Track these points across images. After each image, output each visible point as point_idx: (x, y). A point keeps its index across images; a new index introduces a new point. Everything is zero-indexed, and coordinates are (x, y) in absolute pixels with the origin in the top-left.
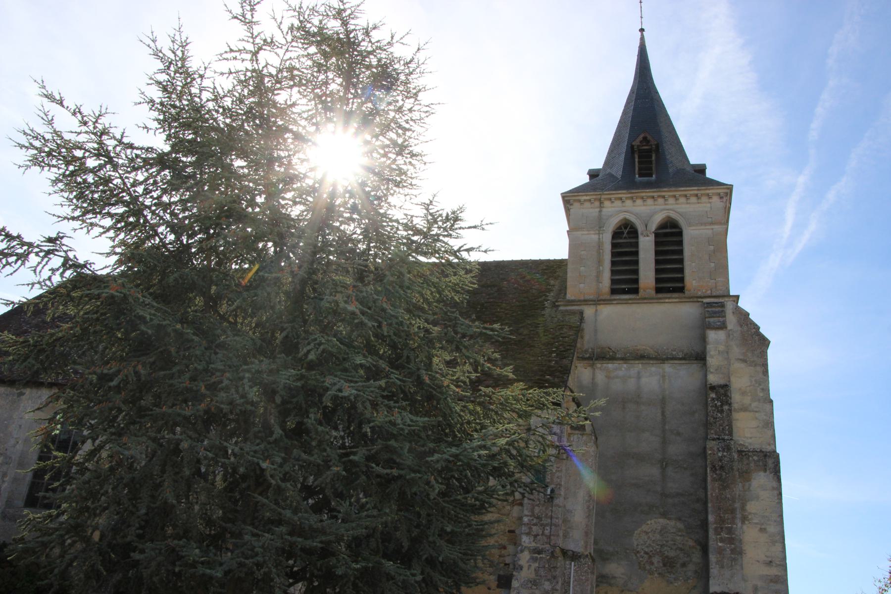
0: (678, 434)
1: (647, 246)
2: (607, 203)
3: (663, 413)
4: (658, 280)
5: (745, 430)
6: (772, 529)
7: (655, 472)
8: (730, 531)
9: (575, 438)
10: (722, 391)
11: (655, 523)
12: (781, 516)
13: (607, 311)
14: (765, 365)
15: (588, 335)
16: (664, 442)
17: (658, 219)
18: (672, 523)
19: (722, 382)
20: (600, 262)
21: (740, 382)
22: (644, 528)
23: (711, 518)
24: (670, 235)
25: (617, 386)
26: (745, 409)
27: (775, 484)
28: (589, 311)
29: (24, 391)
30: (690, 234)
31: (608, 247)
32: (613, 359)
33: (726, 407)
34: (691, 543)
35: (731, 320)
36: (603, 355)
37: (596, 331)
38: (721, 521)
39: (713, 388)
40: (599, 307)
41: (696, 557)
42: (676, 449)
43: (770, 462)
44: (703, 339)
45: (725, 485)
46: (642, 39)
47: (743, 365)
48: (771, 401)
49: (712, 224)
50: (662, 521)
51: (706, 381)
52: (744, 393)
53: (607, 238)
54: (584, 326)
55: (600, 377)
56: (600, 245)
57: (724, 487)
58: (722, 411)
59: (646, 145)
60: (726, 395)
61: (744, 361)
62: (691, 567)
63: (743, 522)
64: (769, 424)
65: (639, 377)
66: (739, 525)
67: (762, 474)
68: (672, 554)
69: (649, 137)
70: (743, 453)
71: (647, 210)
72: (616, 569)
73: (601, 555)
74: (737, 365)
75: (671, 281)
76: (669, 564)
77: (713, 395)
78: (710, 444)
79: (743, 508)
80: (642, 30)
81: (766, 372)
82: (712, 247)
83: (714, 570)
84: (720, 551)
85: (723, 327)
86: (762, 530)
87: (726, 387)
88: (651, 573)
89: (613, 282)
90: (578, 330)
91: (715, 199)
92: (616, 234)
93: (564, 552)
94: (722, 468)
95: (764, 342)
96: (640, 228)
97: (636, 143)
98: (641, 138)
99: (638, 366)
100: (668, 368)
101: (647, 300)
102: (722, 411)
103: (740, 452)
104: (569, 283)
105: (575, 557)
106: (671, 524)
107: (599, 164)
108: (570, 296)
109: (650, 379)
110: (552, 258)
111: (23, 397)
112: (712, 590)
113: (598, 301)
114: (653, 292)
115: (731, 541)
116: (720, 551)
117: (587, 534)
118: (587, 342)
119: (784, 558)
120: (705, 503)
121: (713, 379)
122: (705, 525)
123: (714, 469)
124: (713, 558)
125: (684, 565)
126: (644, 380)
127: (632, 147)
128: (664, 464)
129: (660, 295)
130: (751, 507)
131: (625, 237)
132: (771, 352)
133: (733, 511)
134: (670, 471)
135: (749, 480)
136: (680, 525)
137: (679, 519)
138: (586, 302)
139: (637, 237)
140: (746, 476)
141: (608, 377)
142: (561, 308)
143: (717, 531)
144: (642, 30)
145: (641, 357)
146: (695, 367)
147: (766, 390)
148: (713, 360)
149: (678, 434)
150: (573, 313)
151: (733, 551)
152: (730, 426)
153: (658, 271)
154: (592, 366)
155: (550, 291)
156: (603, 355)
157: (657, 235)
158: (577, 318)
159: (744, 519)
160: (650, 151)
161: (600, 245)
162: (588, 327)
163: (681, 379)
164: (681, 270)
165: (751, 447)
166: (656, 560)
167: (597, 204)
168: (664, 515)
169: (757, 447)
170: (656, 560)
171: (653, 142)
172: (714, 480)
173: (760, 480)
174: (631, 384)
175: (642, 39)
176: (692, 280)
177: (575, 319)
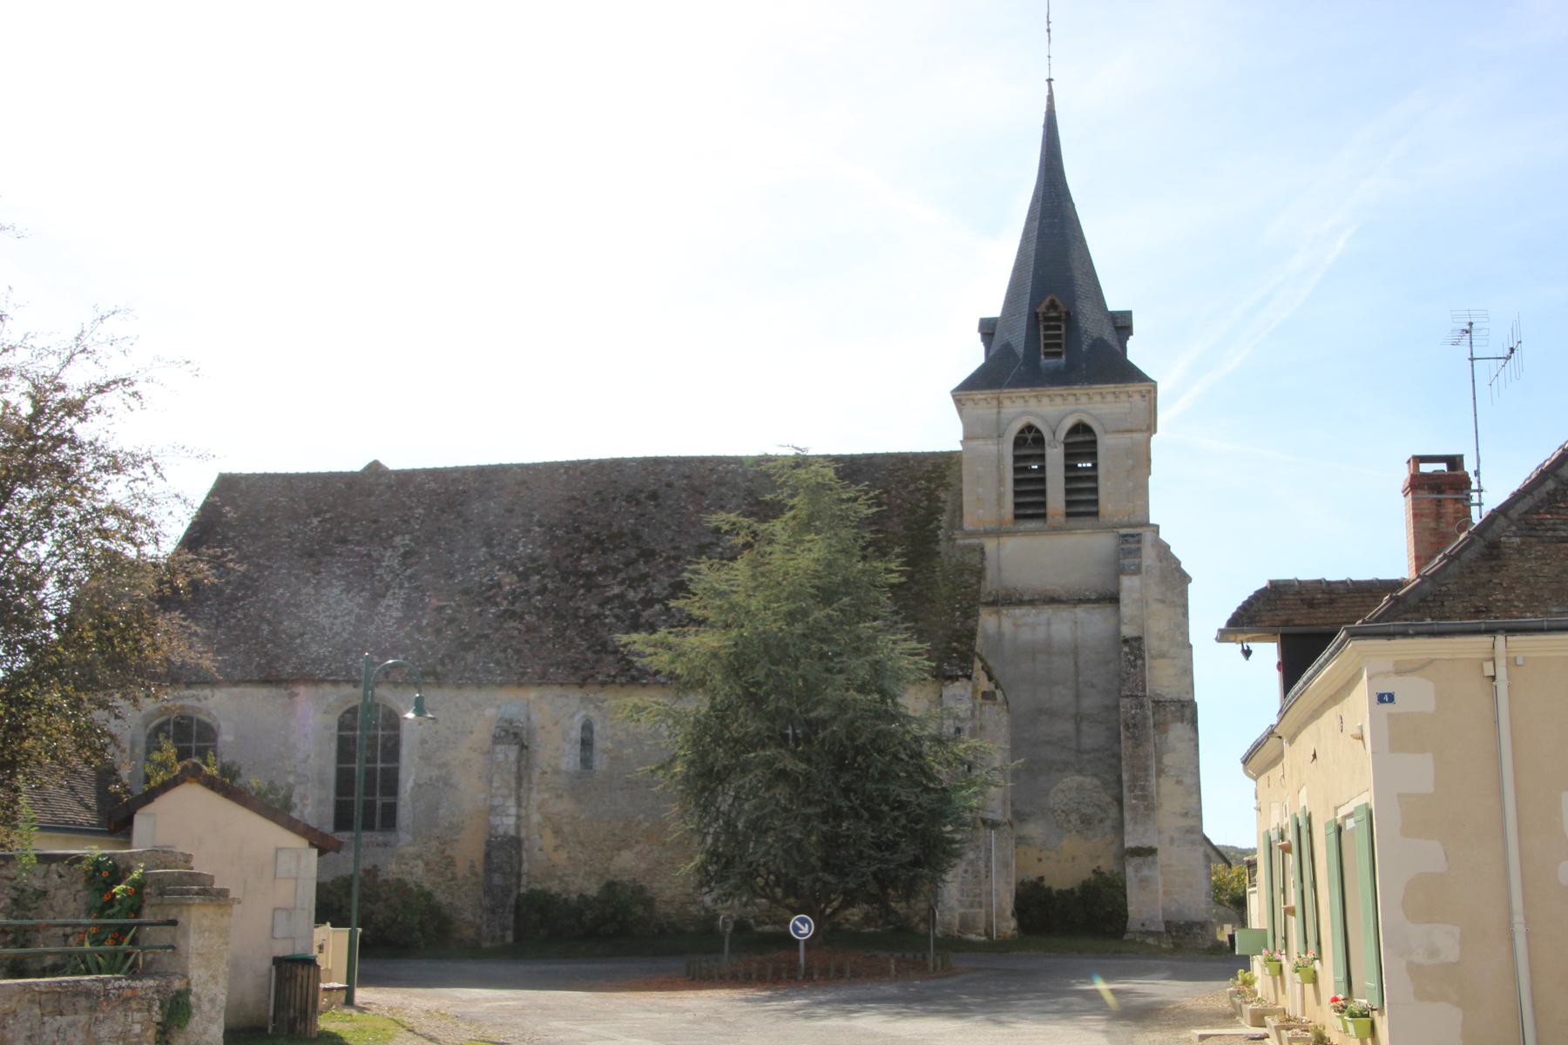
0: (1093, 686)
1: (1055, 456)
2: (1007, 403)
3: (1076, 663)
4: (1069, 503)
5: (1160, 679)
6: (1188, 780)
7: (1069, 727)
8: (1143, 788)
9: (986, 708)
10: (1135, 644)
11: (1072, 780)
12: (1198, 767)
13: (1011, 544)
14: (1185, 607)
15: (990, 574)
16: (1078, 696)
17: (1069, 423)
18: (1088, 780)
19: (1135, 634)
20: (1001, 482)
21: (1157, 627)
22: (1060, 786)
23: (1125, 777)
24: (1082, 441)
25: (1025, 635)
26: (1163, 656)
27: (1192, 735)
28: (990, 545)
29: (296, 690)
30: (1105, 443)
31: (1009, 476)
32: (1021, 603)
33: (1139, 662)
34: (1108, 799)
35: (1149, 556)
36: (1008, 600)
37: (999, 569)
38: (1134, 778)
39: (1126, 641)
40: (1004, 540)
41: (1113, 812)
42: (1091, 702)
43: (1188, 712)
44: (1118, 584)
45: (1138, 742)
46: (1050, 98)
47: (1160, 606)
48: (1190, 646)
49: (1131, 431)
50: (1079, 778)
51: (1118, 631)
52: (1161, 638)
53: (1008, 449)
54: (987, 564)
55: (1007, 625)
56: (1000, 457)
57: (1137, 746)
58: (1135, 667)
59: (1058, 328)
60: (1139, 649)
61: (1163, 602)
62: (1108, 823)
63: (1158, 775)
64: (1187, 672)
65: (1049, 624)
66: (1154, 781)
67: (1179, 725)
68: (1089, 811)
69: (1058, 302)
70: (1158, 703)
71: (1053, 410)
72: (1033, 829)
73: (1019, 817)
74: (1156, 607)
75: (1083, 500)
76: (1086, 821)
77: (1126, 649)
78: (1124, 702)
79: (1159, 761)
80: (1050, 80)
81: (1185, 614)
82: (1130, 462)
83: (1128, 827)
84: (1134, 808)
85: (1137, 571)
86: (1179, 782)
87: (1139, 639)
88: (1069, 831)
89: (1017, 505)
90: (980, 573)
91: (1137, 397)
92: (1019, 442)
93: (984, 822)
94: (1135, 726)
95: (1185, 579)
96: (1047, 436)
97: (1041, 309)
98: (1046, 302)
99: (1048, 612)
100: (1080, 612)
101: (1056, 530)
102: (1135, 667)
103: (1157, 703)
104: (967, 508)
105: (994, 825)
106: (1088, 781)
107: (995, 310)
108: (968, 524)
109: (1061, 625)
110: (937, 450)
111: (297, 699)
112: (1127, 845)
113: (998, 533)
114: (1062, 519)
115: (1144, 798)
116: (1134, 808)
117: (1004, 803)
118: (990, 585)
119: (1200, 809)
120: (1120, 759)
121: (1127, 631)
122: (1119, 781)
123: (1127, 727)
124: (1127, 815)
125: (1101, 821)
126: (1054, 627)
127: (1036, 315)
128: (1078, 718)
129: (1073, 522)
130: (1168, 760)
131: (1030, 440)
132: (1192, 589)
133: (1146, 769)
134: (1084, 726)
135: (1165, 732)
136: (1096, 781)
137: (1095, 775)
138: (987, 533)
139: (1043, 447)
140: (1161, 727)
141: (1016, 625)
142: (960, 542)
143: (1132, 789)
144: (1050, 80)
145: (1052, 600)
146: (1109, 610)
147: (1186, 634)
148: (1127, 608)
149: (1093, 686)
150: (972, 549)
151: (1146, 808)
152: (1144, 681)
153: (1068, 492)
154: (998, 612)
155: (942, 511)
156: (1008, 600)
157: (1067, 445)
158: (978, 558)
159: (1160, 772)
160: (1058, 319)
161: (1000, 457)
162: (990, 565)
163: (1092, 624)
164: (1095, 490)
165: (1168, 697)
166: (1073, 817)
167: (995, 402)
168: (1080, 772)
169: (1175, 696)
170: (1073, 817)
171: (1063, 309)
172: (1128, 738)
173: (1177, 731)
174: (1041, 633)
175: (1050, 90)
176: (1108, 503)
177: (974, 559)
